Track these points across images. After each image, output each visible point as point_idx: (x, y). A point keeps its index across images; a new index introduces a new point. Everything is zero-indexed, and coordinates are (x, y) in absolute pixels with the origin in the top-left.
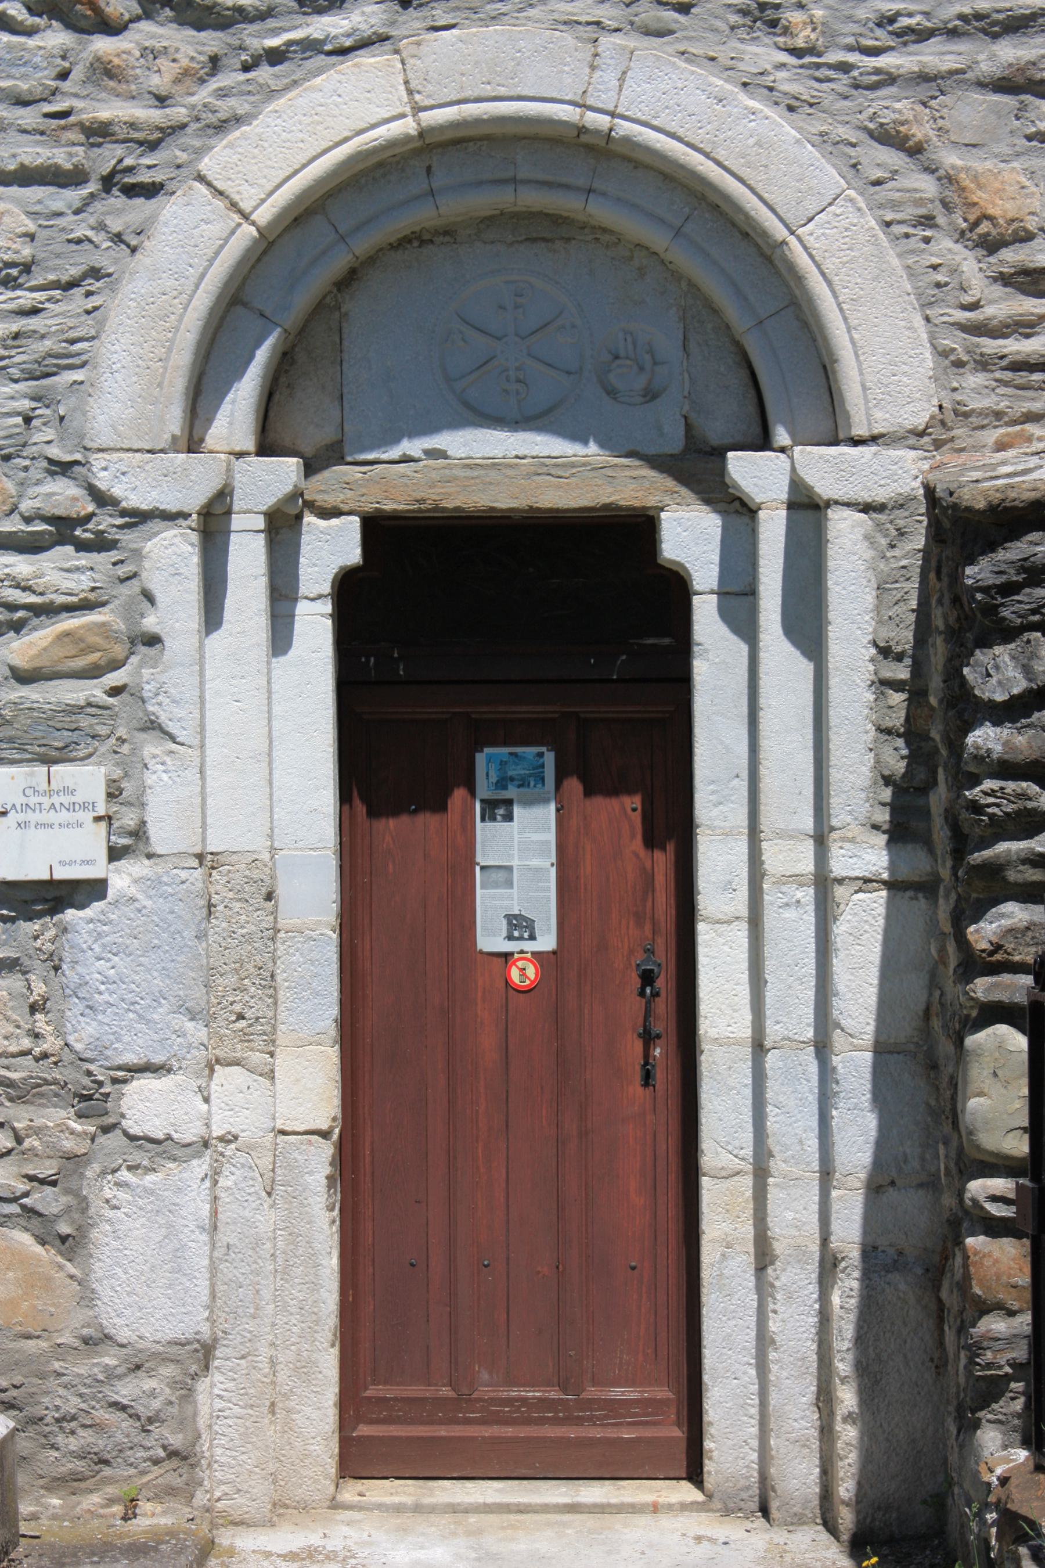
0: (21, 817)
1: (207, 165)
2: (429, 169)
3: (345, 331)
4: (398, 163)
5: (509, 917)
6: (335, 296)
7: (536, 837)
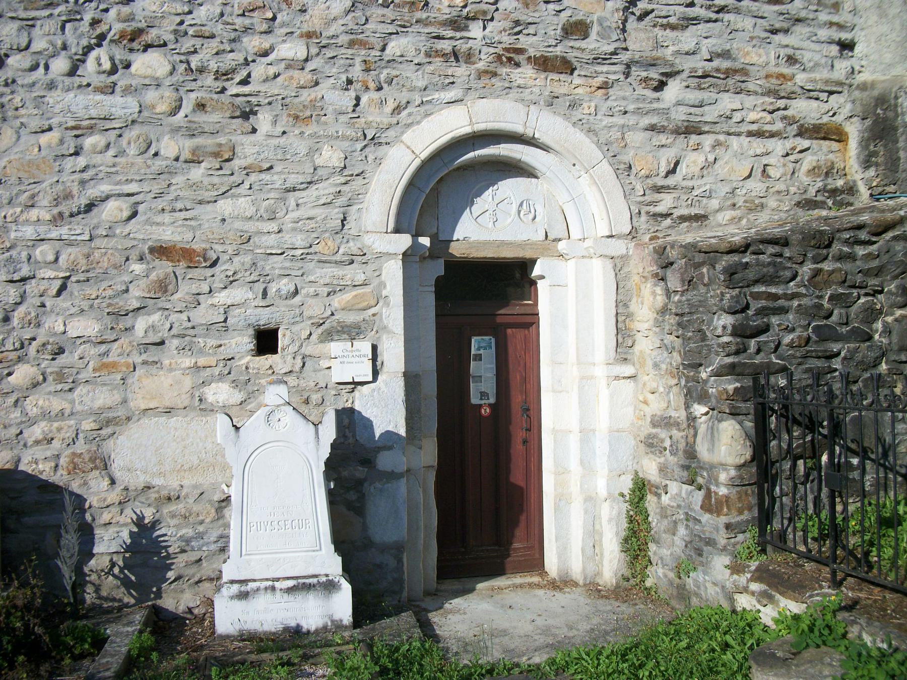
0: (342, 360)
1: (405, 137)
5: (481, 393)
7: (489, 366)
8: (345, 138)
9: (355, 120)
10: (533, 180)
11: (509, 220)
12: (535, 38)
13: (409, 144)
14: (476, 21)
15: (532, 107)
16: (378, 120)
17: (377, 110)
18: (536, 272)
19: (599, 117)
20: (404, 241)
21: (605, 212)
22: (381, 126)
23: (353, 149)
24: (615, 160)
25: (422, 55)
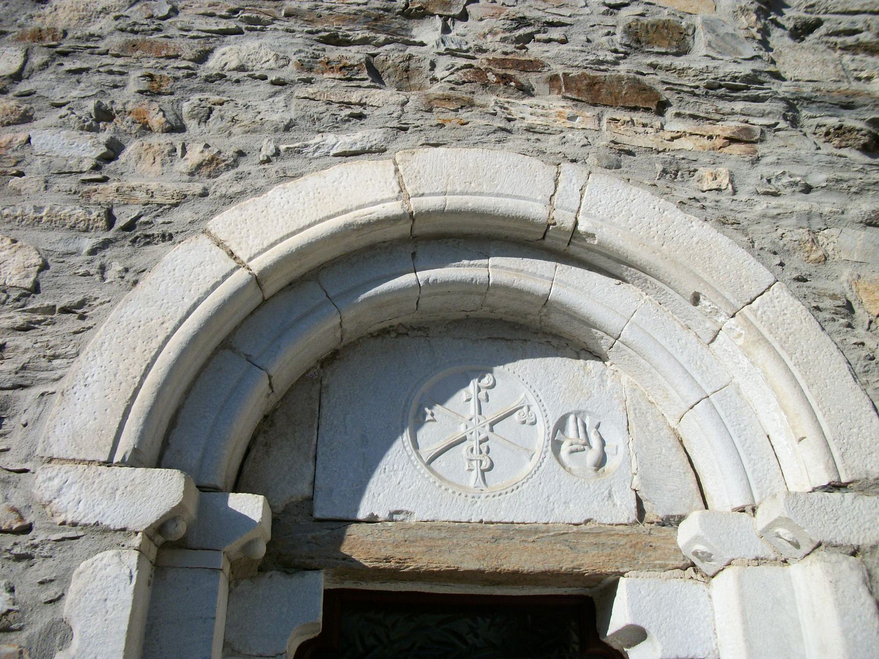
2: (414, 254)
3: (325, 403)
4: (387, 248)
6: (318, 371)
8: (55, 223)
9: (93, 187)
10: (591, 364)
11: (529, 466)
12: (564, 47)
13: (222, 236)
14: (426, 21)
15: (566, 167)
16: (153, 186)
17: (157, 167)
18: (620, 616)
19: (742, 196)
20: (162, 491)
21: (805, 416)
22: (159, 199)
23: (72, 248)
24: (804, 288)
25: (291, 67)
